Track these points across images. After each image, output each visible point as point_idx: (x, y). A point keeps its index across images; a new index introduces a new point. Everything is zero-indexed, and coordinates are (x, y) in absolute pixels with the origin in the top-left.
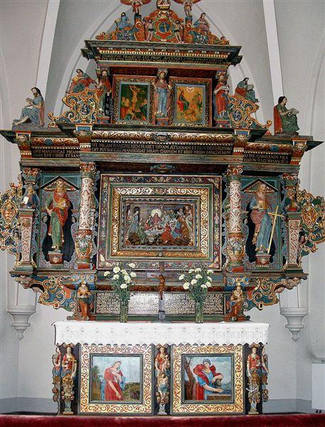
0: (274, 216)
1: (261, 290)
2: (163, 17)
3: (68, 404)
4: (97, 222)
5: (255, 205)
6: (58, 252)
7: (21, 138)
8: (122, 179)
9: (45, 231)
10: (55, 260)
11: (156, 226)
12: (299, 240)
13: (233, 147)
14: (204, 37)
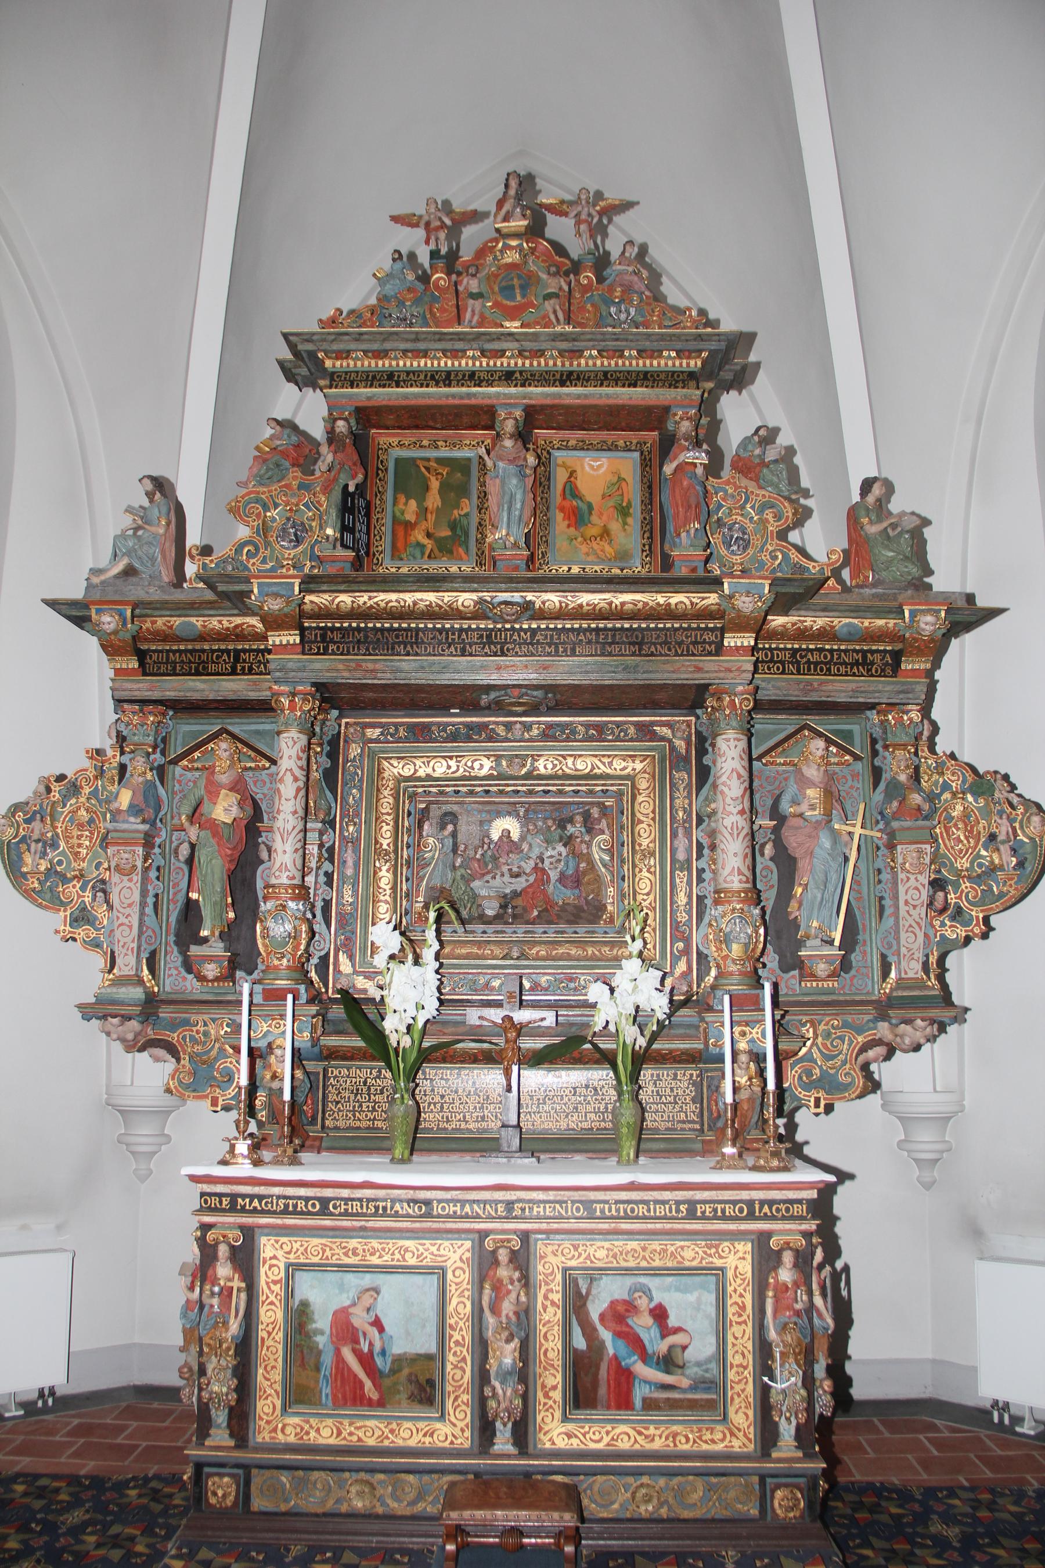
0: (850, 834)
1: (816, 1054)
2: (511, 257)
3: (220, 1417)
4: (331, 860)
5: (795, 802)
6: (217, 948)
7: (108, 621)
8: (402, 733)
9: (184, 884)
10: (211, 970)
11: (505, 868)
12: (930, 904)
13: (723, 631)
14: (632, 311)
